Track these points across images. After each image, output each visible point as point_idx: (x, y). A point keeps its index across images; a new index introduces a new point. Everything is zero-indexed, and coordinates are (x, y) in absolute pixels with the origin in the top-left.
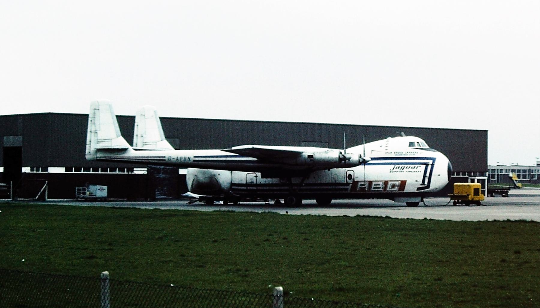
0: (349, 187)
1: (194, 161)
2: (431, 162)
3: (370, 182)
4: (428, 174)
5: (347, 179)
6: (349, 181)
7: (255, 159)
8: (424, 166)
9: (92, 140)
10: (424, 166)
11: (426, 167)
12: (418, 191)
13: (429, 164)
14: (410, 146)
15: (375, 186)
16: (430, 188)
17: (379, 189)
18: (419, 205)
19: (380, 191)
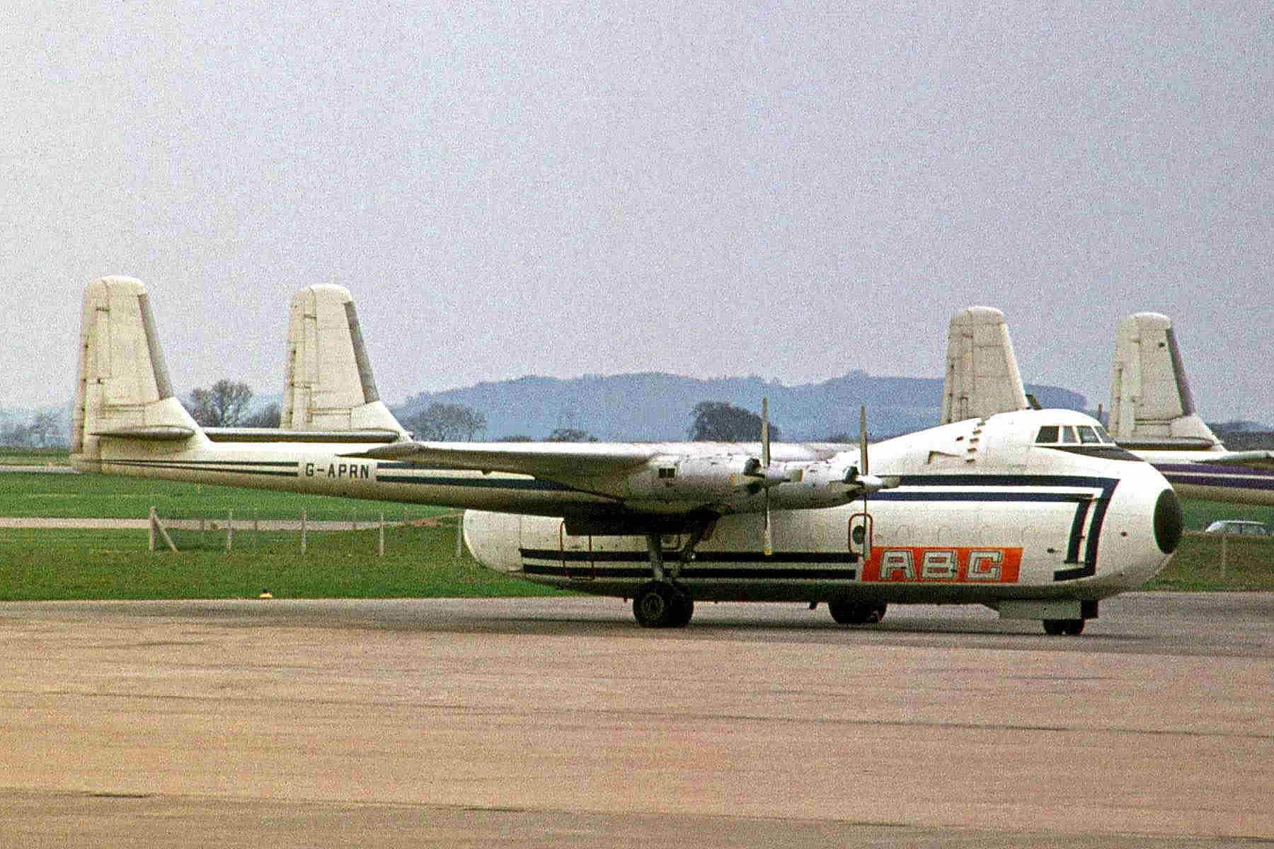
0: (859, 567)
1: (380, 478)
2: (1097, 492)
3: (918, 554)
4: (1086, 531)
5: (852, 540)
6: (857, 548)
7: (531, 478)
8: (1073, 507)
9: (297, 350)
10: (1073, 507)
11: (1080, 507)
12: (1059, 583)
13: (1091, 501)
14: (1039, 440)
15: (930, 565)
16: (1097, 572)
17: (945, 575)
18: (1085, 631)
19: (944, 579)
